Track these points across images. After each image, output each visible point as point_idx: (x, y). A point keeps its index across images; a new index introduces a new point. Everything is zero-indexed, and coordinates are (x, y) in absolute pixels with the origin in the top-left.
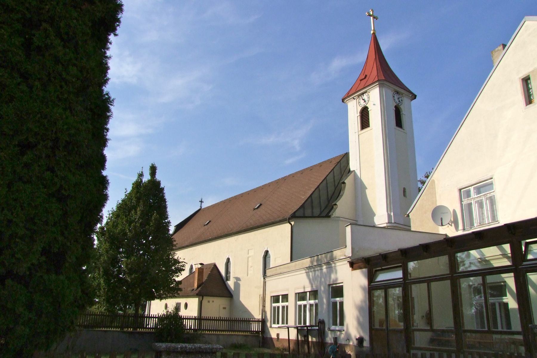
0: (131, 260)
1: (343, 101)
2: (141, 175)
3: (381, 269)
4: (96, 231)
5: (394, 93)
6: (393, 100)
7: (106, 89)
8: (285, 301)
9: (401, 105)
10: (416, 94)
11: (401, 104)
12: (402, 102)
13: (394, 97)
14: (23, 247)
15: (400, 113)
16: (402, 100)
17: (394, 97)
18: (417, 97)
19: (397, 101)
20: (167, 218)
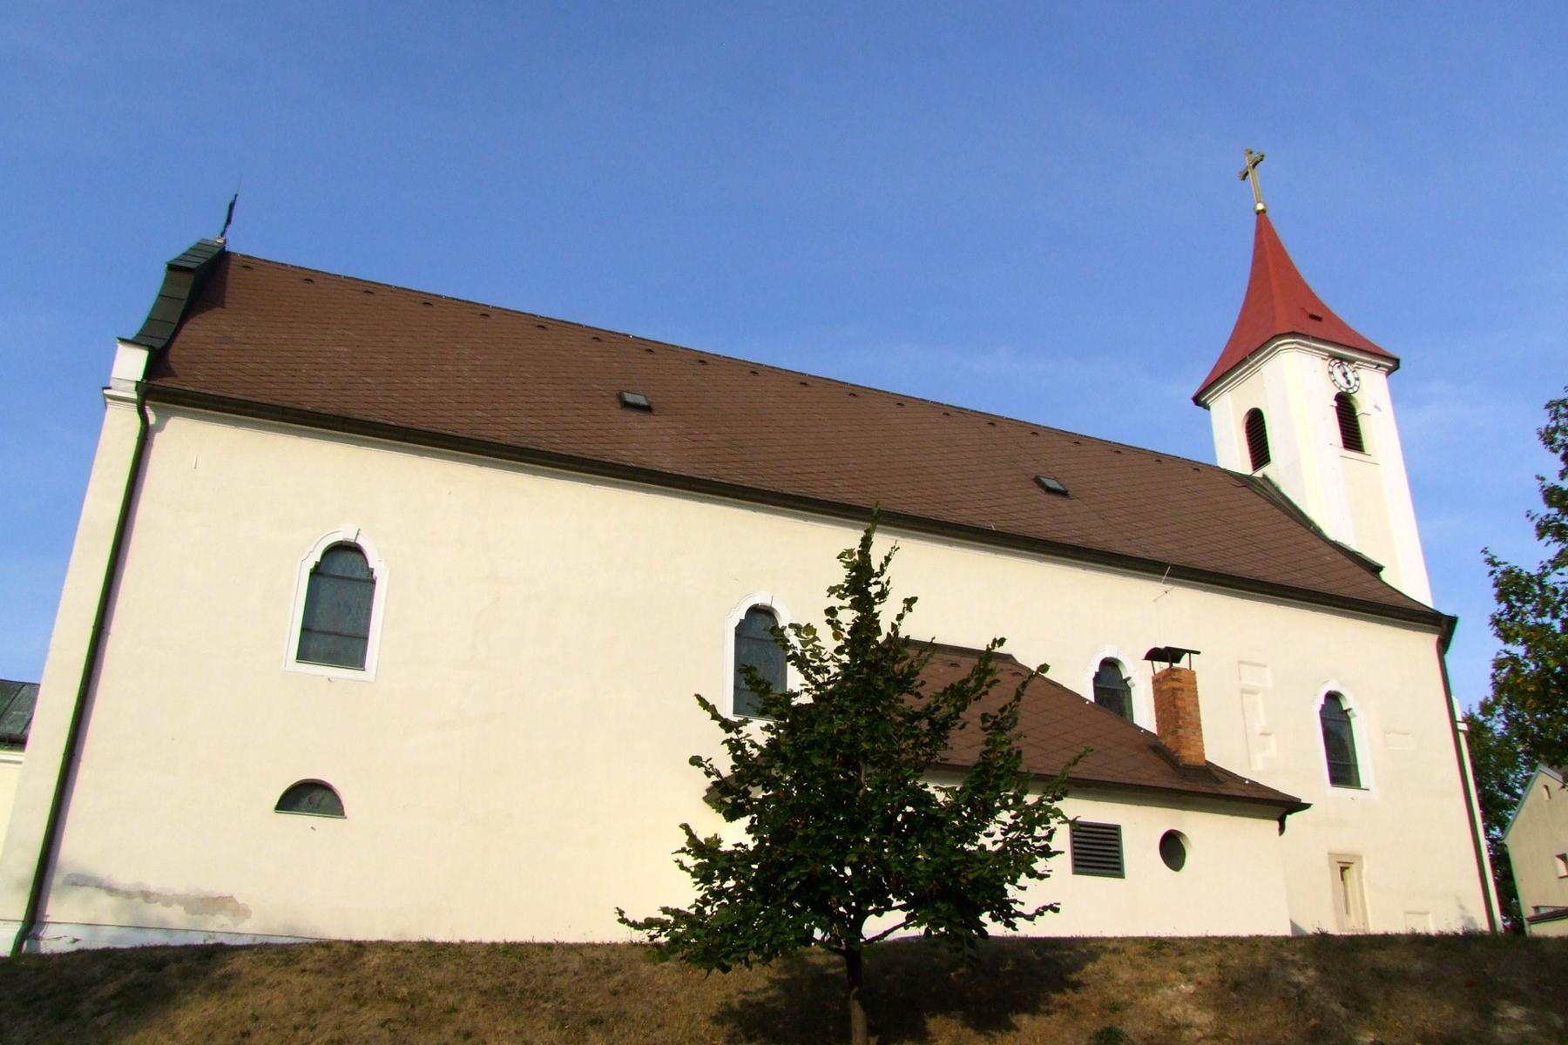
0: (725, 886)
1: (1199, 400)
2: (1548, 543)
3: (1515, 618)
4: (925, 1014)
5: (1330, 365)
6: (1332, 384)
7: (1460, 933)
8: (1200, 743)
9: (1355, 392)
10: (1396, 355)
11: (1355, 389)
12: (1357, 383)
13: (1331, 373)
14: (100, 1040)
15: (1355, 413)
16: (1357, 379)
17: (1331, 373)
18: (1401, 364)
19: (1342, 381)
20: (724, 815)
